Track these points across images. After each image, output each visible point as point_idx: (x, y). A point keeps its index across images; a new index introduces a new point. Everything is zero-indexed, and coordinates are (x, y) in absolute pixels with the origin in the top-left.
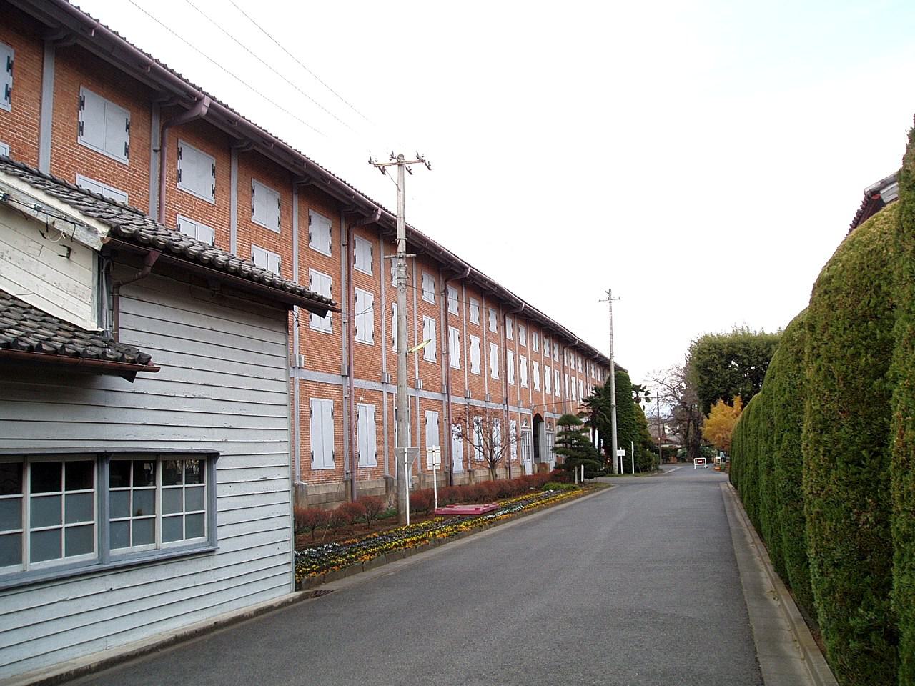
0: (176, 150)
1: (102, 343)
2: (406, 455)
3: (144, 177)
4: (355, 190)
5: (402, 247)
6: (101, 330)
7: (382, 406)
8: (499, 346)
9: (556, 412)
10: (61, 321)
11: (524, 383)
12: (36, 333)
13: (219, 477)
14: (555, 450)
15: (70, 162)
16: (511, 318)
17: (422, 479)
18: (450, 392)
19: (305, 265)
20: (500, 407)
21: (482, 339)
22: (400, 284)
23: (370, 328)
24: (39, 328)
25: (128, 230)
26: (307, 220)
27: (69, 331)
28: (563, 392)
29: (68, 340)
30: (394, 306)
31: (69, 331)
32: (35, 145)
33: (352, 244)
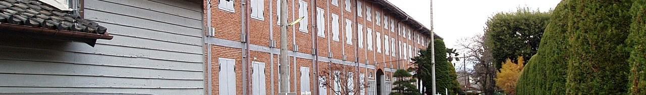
6: (71, 10)
8: (353, 21)
9: (392, 67)
12: (25, 12)
18: (318, 54)
20: (353, 64)
21: (340, 16)
24: (27, 8)
27: (49, 11)
28: (397, 53)
29: (48, 17)
31: (49, 11)
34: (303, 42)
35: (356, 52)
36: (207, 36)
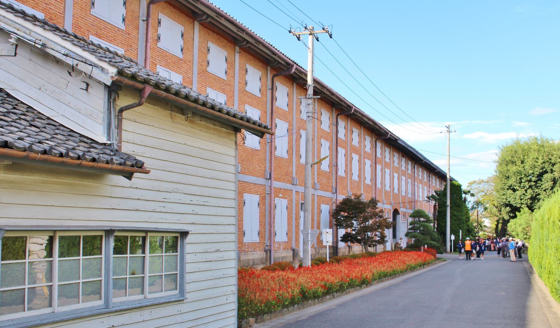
0: (157, 21)
1: (110, 152)
2: (310, 234)
3: (135, 39)
4: (276, 49)
5: (310, 91)
6: (109, 142)
7: (292, 200)
8: (372, 162)
9: (408, 208)
10: (81, 136)
11: (388, 188)
12: (64, 144)
13: (188, 248)
14: (407, 235)
15: (85, 27)
16: (380, 142)
17: (317, 251)
18: (273, 178)
19: (242, 103)
21: (360, 156)
22: (309, 116)
23: (286, 147)
24: (66, 140)
25: (130, 71)
26: (245, 71)
27: (87, 143)
29: (87, 150)
30: (303, 133)
31: (87, 143)
32: (62, 14)
33: (275, 88)
34: (325, 181)
35: (374, 192)
36: (266, 179)
